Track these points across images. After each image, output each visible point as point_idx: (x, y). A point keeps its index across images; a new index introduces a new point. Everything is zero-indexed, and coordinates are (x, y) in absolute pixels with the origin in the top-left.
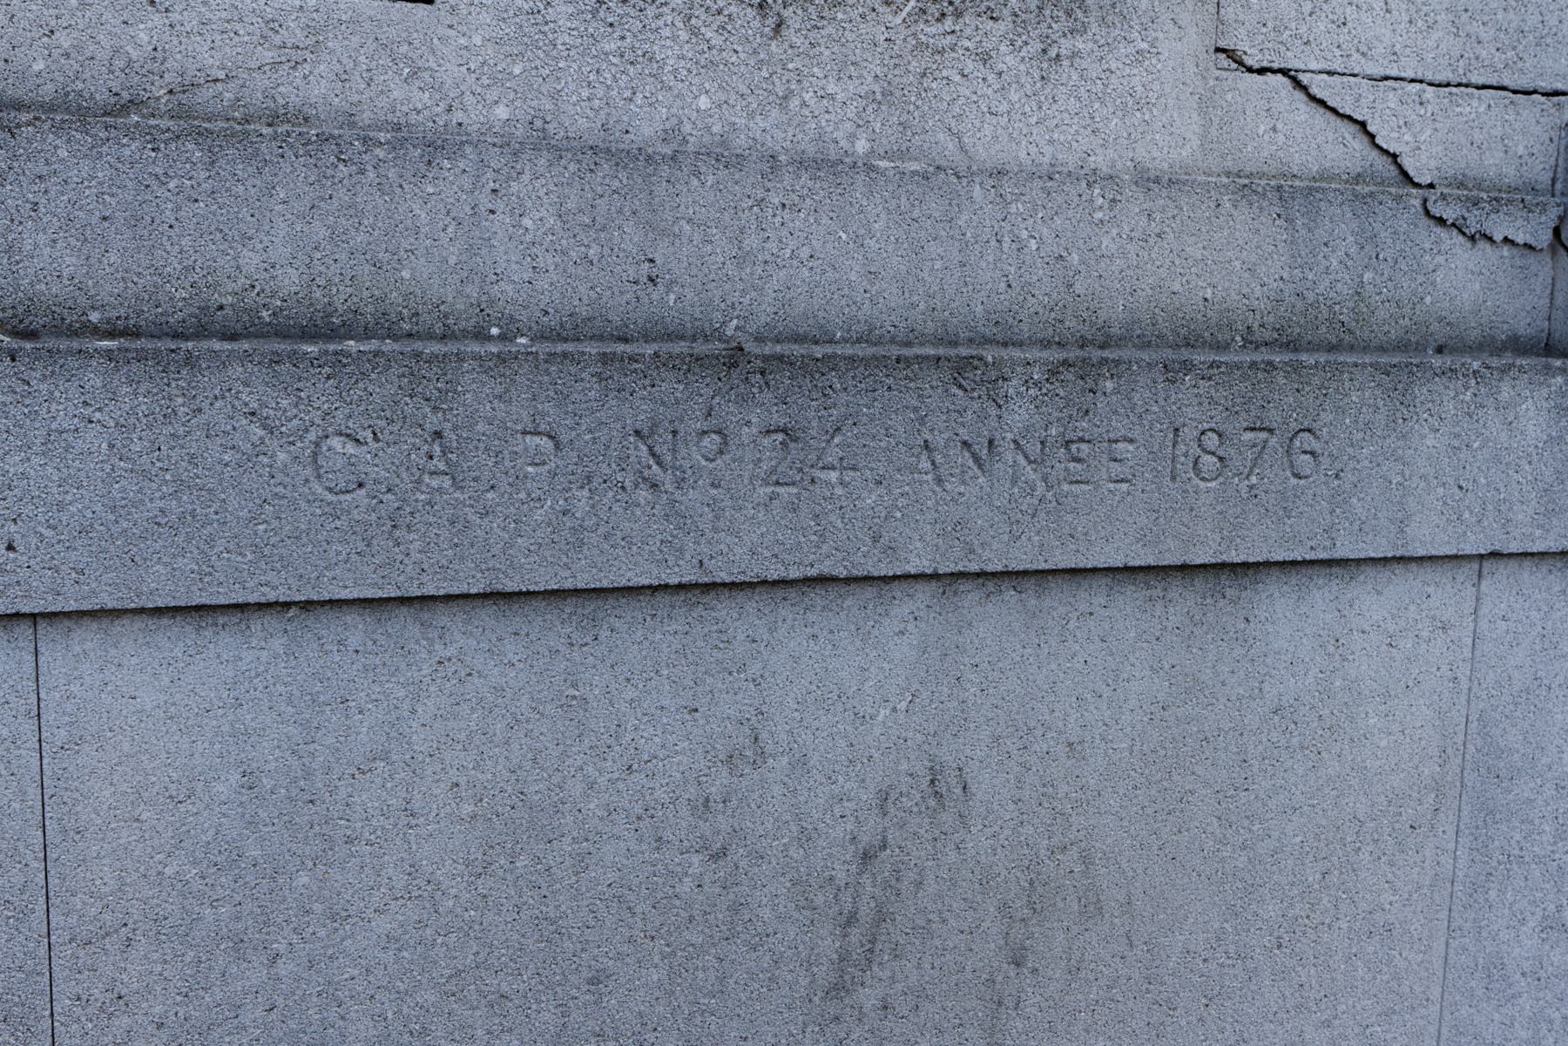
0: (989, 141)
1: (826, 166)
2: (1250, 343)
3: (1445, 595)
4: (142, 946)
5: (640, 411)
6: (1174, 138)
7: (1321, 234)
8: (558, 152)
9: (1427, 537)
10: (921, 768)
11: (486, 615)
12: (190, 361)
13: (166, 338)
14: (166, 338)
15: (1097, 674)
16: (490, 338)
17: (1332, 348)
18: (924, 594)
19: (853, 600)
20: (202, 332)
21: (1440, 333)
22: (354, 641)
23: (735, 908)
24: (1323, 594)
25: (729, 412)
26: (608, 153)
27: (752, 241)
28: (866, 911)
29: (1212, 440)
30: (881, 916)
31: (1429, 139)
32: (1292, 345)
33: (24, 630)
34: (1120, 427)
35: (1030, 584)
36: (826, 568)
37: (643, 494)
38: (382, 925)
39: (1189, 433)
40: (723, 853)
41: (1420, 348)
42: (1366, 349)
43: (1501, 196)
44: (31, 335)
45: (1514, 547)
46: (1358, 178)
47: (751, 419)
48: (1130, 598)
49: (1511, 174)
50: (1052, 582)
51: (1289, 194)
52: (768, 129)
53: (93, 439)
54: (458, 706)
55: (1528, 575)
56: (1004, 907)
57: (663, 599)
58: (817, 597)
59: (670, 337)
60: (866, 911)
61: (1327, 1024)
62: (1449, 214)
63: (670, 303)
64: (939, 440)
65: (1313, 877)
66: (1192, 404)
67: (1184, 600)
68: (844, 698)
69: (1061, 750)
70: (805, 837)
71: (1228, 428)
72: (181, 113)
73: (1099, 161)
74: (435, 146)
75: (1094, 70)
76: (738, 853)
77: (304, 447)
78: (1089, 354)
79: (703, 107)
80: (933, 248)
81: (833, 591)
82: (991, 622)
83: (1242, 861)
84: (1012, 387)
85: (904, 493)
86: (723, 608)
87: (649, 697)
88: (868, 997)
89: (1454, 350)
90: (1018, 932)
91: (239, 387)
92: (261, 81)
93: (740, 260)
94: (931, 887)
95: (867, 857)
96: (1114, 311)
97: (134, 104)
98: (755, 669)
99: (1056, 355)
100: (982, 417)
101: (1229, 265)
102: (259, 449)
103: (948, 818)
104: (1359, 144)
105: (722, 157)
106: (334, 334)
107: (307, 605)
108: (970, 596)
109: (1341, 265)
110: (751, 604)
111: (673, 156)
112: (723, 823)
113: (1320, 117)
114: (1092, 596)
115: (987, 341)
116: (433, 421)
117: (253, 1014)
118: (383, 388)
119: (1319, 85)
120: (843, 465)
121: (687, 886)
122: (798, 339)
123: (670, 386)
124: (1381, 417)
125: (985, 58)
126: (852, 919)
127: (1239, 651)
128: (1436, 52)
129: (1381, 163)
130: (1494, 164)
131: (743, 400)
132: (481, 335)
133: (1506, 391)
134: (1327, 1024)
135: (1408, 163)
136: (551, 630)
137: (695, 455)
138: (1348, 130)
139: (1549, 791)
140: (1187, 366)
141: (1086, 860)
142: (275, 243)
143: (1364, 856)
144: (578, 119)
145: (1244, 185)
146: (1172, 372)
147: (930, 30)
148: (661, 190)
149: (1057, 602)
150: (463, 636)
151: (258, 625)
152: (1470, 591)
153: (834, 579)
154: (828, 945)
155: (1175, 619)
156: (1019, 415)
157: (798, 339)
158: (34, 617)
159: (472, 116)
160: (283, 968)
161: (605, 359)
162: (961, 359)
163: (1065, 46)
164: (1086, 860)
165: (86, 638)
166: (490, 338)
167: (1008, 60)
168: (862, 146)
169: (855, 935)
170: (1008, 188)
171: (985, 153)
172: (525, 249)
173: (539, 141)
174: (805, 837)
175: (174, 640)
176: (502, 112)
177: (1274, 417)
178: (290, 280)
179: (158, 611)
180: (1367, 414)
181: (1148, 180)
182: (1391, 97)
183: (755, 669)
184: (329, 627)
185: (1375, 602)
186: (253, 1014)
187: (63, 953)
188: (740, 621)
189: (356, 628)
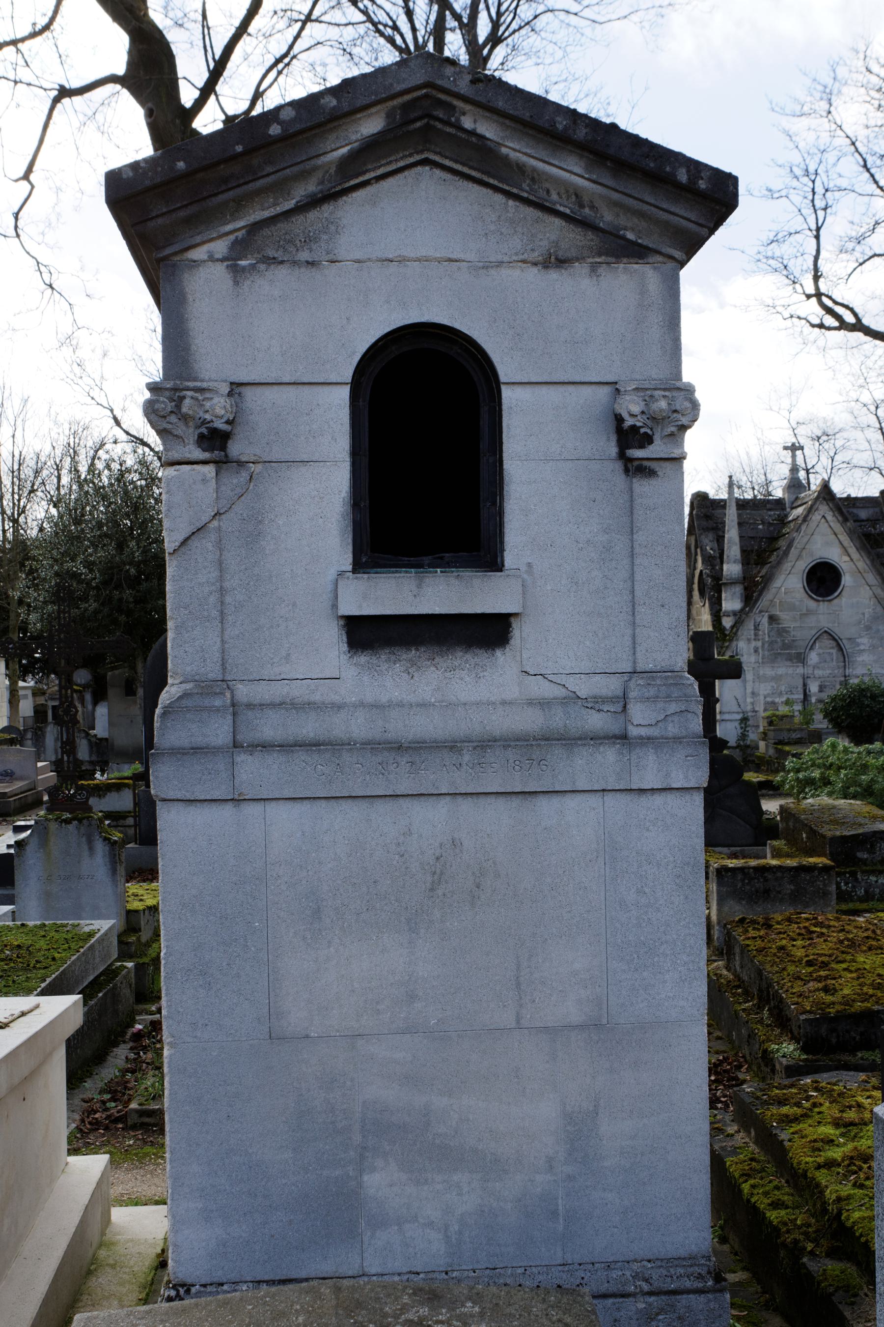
0: (463, 697)
1: (423, 705)
2: (535, 739)
3: (594, 801)
4: (283, 866)
5: (380, 759)
6: (512, 692)
7: (553, 712)
8: (364, 707)
9: (580, 786)
10: (450, 838)
11: (350, 801)
12: (292, 751)
13: (288, 747)
14: (288, 747)
15: (496, 817)
16: (848, 873)
17: (558, 740)
18: (448, 798)
19: (432, 799)
20: (295, 745)
21: (592, 735)
22: (323, 806)
23: (407, 868)
24: (556, 800)
25: (399, 759)
26: (376, 706)
27: (407, 722)
28: (438, 871)
29: (517, 763)
30: (442, 873)
31: (584, 688)
32: (547, 739)
33: (262, 802)
34: (493, 760)
35: (474, 796)
36: (422, 792)
37: (381, 776)
38: (329, 865)
39: (511, 761)
40: (402, 856)
41: (585, 739)
42: (569, 739)
43: (605, 700)
44: (265, 747)
45: (609, 788)
46: (565, 698)
47: (403, 760)
48: (501, 801)
49: (610, 694)
50: (481, 796)
51: (544, 704)
52: (412, 698)
53: (275, 766)
54: (342, 820)
55: (618, 795)
56: (473, 873)
57: (387, 798)
58: (422, 798)
59: (390, 743)
60: (438, 871)
61: (569, 912)
62: (589, 706)
63: (389, 736)
64: (447, 764)
65: (561, 872)
66: (510, 754)
67: (515, 802)
68: (430, 821)
69: (486, 836)
70: (422, 853)
71: (522, 760)
72: (292, 704)
73: (492, 699)
74: (338, 707)
75: (490, 679)
76: (406, 856)
77: (313, 767)
78: (484, 744)
79: (397, 695)
80: (450, 722)
81: (426, 798)
82: (465, 805)
83: (539, 866)
84: (464, 752)
85: (439, 775)
86: (401, 801)
87: (385, 820)
88: (440, 892)
89: (596, 739)
90: (477, 880)
91: (301, 756)
92: (307, 697)
93: (405, 727)
94: (454, 867)
95: (437, 859)
96: (497, 733)
97: (284, 703)
98: (409, 814)
99: (475, 744)
100: (457, 758)
101: (529, 721)
102: (304, 768)
103: (457, 851)
104: (564, 690)
105: (401, 705)
106: (320, 745)
107: (314, 798)
108: (460, 799)
109: (558, 720)
110: (408, 800)
111: (390, 705)
112: (403, 848)
113: (552, 685)
114: (491, 800)
115: (464, 741)
116: (337, 762)
117: (304, 882)
118: (328, 755)
119: (550, 677)
120: (424, 769)
121: (395, 862)
122: (418, 743)
123: (386, 754)
124: (565, 756)
125: (462, 679)
126: (435, 873)
127: (533, 814)
128: (586, 666)
129: (571, 694)
130: (604, 692)
131: (402, 756)
132: (349, 744)
133: (602, 749)
134: (569, 912)
135: (578, 693)
136: (364, 804)
137: (392, 768)
138: (560, 687)
139: (634, 854)
140: (509, 746)
141: (494, 863)
142: (308, 727)
143: (576, 867)
144: (369, 698)
145: (530, 703)
146: (505, 747)
147: (448, 674)
148: (386, 713)
149: (482, 800)
150: (345, 805)
151: (305, 802)
152: (600, 799)
153: (424, 795)
154: (429, 879)
155: (514, 806)
156: (466, 758)
157: (418, 743)
158: (264, 799)
159: (348, 700)
160: (310, 873)
161: (372, 748)
162: (453, 746)
163: (481, 674)
164: (494, 863)
165: (273, 804)
166: (848, 873)
167: (467, 679)
168: (433, 700)
169: (436, 877)
170: (467, 707)
171: (463, 700)
172: (358, 726)
173: (362, 704)
174: (422, 853)
175: (289, 805)
176: (354, 699)
177: (534, 757)
178: (312, 735)
179: (286, 799)
180: (560, 756)
181: (504, 703)
182: (571, 679)
183: (409, 814)
184: (319, 803)
185: (571, 802)
186: (304, 882)
187: (269, 866)
188: (405, 803)
189: (323, 803)
